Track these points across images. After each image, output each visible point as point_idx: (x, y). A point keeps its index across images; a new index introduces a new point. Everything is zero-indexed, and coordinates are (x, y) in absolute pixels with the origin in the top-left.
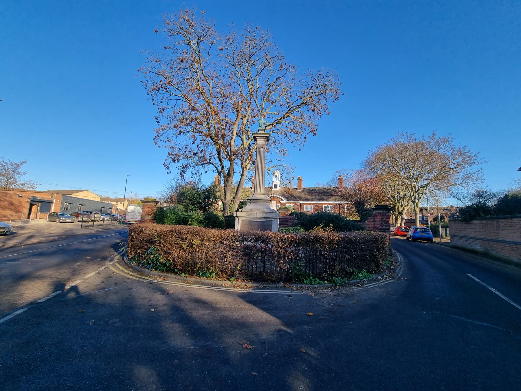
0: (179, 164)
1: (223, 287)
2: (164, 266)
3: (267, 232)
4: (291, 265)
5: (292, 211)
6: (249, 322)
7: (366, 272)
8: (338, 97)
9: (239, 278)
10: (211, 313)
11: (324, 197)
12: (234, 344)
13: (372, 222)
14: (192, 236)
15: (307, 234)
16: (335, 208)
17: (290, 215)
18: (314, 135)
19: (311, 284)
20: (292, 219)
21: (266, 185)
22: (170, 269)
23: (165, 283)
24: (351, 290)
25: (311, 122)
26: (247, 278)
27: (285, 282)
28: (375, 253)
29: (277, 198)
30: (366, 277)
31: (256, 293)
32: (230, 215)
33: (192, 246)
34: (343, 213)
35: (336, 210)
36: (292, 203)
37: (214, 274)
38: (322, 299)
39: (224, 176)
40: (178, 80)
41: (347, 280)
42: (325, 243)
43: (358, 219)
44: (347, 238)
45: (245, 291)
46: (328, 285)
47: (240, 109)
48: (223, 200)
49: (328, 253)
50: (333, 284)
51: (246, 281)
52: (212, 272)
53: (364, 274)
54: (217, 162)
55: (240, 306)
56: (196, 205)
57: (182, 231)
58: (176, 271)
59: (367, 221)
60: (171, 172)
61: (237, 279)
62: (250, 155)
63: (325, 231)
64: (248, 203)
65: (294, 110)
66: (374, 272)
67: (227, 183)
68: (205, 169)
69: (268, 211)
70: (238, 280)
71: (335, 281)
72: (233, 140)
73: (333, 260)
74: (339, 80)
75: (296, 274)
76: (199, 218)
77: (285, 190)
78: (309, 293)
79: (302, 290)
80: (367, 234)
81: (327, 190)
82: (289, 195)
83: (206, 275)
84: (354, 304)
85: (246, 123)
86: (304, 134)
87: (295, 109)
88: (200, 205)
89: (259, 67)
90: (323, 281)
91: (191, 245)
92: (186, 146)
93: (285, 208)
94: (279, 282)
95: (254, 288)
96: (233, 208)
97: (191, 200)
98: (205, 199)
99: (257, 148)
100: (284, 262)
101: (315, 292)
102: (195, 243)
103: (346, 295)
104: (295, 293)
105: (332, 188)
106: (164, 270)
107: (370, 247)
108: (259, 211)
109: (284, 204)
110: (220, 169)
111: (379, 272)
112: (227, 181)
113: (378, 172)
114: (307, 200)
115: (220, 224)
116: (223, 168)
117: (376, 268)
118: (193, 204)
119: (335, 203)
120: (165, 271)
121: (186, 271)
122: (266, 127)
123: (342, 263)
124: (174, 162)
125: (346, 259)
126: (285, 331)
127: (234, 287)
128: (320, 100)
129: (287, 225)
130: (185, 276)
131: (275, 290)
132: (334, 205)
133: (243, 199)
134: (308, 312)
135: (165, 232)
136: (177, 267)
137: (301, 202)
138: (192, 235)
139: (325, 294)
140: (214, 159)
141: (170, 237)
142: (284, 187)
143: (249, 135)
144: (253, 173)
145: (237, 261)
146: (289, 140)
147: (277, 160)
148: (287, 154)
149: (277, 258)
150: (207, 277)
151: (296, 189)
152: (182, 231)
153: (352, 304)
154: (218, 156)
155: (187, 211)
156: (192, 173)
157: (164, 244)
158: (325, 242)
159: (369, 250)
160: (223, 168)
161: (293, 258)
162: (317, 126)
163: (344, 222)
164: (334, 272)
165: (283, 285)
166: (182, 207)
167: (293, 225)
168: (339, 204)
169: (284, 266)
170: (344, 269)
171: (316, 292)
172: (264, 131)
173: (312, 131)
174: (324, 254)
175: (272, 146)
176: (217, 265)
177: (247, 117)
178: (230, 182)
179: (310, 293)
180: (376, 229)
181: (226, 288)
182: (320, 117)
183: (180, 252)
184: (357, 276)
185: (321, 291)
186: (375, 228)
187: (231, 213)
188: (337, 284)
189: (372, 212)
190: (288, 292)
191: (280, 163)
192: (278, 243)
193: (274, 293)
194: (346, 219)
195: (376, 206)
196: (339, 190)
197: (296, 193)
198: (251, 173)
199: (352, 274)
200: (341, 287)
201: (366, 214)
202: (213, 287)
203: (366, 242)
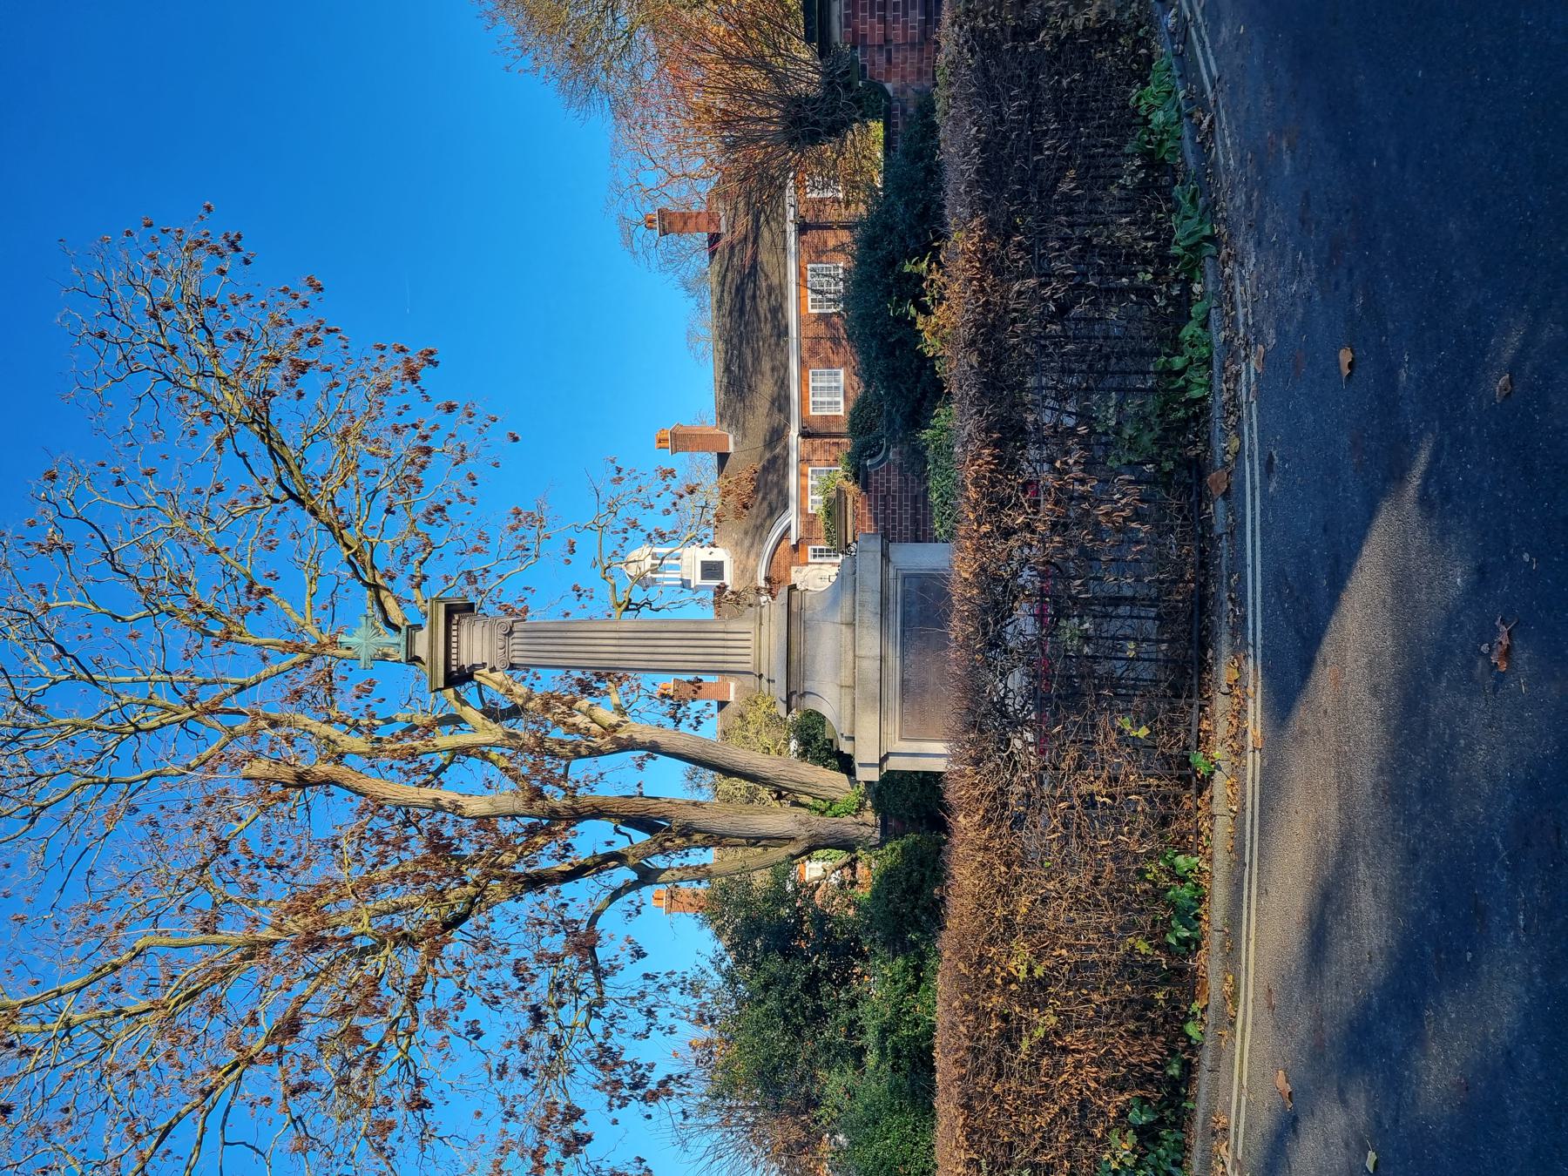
0: (592, 1102)
1: (1244, 810)
2: (1156, 1140)
3: (957, 591)
4: (1116, 464)
5: (846, 477)
6: (1394, 657)
7: (1142, 88)
8: (226, 236)
9: (1194, 730)
10: (1366, 853)
11: (763, 307)
12: (1493, 717)
13: (889, 61)
14: (988, 986)
15: (961, 388)
16: (824, 252)
17: (865, 487)
18: (431, 362)
19: (1208, 363)
20: (888, 474)
21: (709, 613)
22: (1167, 1107)
23: (1242, 1121)
24: (1232, 162)
25: (363, 382)
26: (1190, 690)
27: (1203, 497)
28: (1048, 48)
29: (774, 564)
30: (1166, 88)
31: (1264, 638)
32: (877, 808)
33: (1042, 984)
34: (848, 204)
35: (831, 243)
36: (803, 481)
37: (1180, 860)
38: (1275, 304)
39: (663, 851)
40: (114, 1135)
41: (1183, 183)
42: (1002, 298)
43: (877, 128)
44: (971, 185)
45: (1255, 692)
46: (1210, 278)
47: (290, 770)
48: (794, 851)
49: (1050, 284)
50: (1205, 253)
51: (1207, 692)
52: (1171, 871)
53: (1155, 98)
54: (582, 895)
55: (1325, 712)
56: (825, 1004)
57: (967, 1043)
58: (1174, 1071)
59: (888, 86)
60: (641, 1160)
61: (1199, 742)
62: (546, 707)
63: (942, 298)
64: (810, 704)
65: (296, 472)
66: (1143, 51)
67: (698, 831)
68: (625, 959)
69: (846, 602)
70: (1205, 731)
71: (1189, 242)
72: (462, 800)
73: (1082, 257)
74: (129, 233)
75: (1160, 441)
76: (896, 982)
77: (730, 517)
78: (1252, 371)
79: (1238, 407)
80: (951, 84)
81: (726, 294)
82: (760, 495)
83: (1187, 903)
84: (1292, 147)
85: (362, 738)
86: (429, 416)
87: (288, 466)
88: (820, 980)
89: (44, 669)
90: (1190, 303)
91: (1036, 991)
92: (494, 1077)
93: (829, 514)
94: (1207, 525)
95: (1238, 650)
96: (833, 795)
97: (798, 1031)
98: (788, 953)
99: (512, 666)
100: (1101, 501)
101: (1247, 344)
102: (1023, 968)
103: (1253, 190)
104: (1256, 440)
105: (717, 268)
106: (1176, 1141)
107: (1018, 72)
108: (850, 646)
109: (809, 521)
110: (624, 875)
111: (1140, 26)
112: (687, 831)
113: (624, 21)
114: (781, 402)
115: (921, 863)
116: (620, 858)
117: (1121, 41)
118: (819, 1014)
119: (793, 250)
120: (1179, 1136)
121: (1177, 1017)
122: (389, 624)
123: (1101, 208)
124: (583, 1140)
125: (1079, 192)
126: (1426, 477)
127: (1239, 753)
128: (238, 334)
129: (920, 500)
130: (1202, 1020)
131: (1244, 540)
132: (806, 257)
133: (788, 741)
134: (1340, 372)
135: (976, 1137)
136: (1153, 1064)
137: (794, 433)
138: (983, 987)
139: (1254, 290)
140: (565, 905)
141: (1001, 1108)
142: (719, 521)
143: (431, 717)
144: (642, 692)
145: (1105, 741)
146: (463, 499)
147: (568, 562)
148: (540, 508)
149: (1085, 536)
150: (1200, 901)
151: (723, 458)
152: (967, 1043)
153: (1293, 159)
154: (550, 890)
155: (861, 1051)
156: (649, 1030)
157: (1038, 1141)
158: (996, 298)
159: (1032, 74)
160: (620, 858)
161: (1080, 457)
162: (383, 348)
163: (892, 204)
164: (1146, 248)
165: (1221, 503)
166: (834, 1083)
167: (917, 468)
168: (803, 228)
169: (1123, 502)
170: (1130, 202)
171: (1245, 335)
172: (419, 627)
173: (413, 375)
174: (1054, 300)
175: (495, 592)
176: (1134, 847)
177: (333, 732)
178: (699, 818)
179: (1253, 364)
180: (926, 41)
181: (1249, 794)
182: (336, 330)
183: (1073, 1051)
184: (1162, 133)
185: (1241, 311)
186: (921, 43)
187: (862, 805)
188: (1207, 232)
189: (839, 56)
190: (1252, 472)
191: (587, 545)
192: (1007, 533)
193: (1258, 544)
194: (881, 190)
195: (809, 39)
196: (723, 229)
197: (746, 452)
198: (642, 704)
199: (1152, 162)
200: (1220, 216)
201: (848, 87)
202: (1247, 861)
203: (989, 91)
